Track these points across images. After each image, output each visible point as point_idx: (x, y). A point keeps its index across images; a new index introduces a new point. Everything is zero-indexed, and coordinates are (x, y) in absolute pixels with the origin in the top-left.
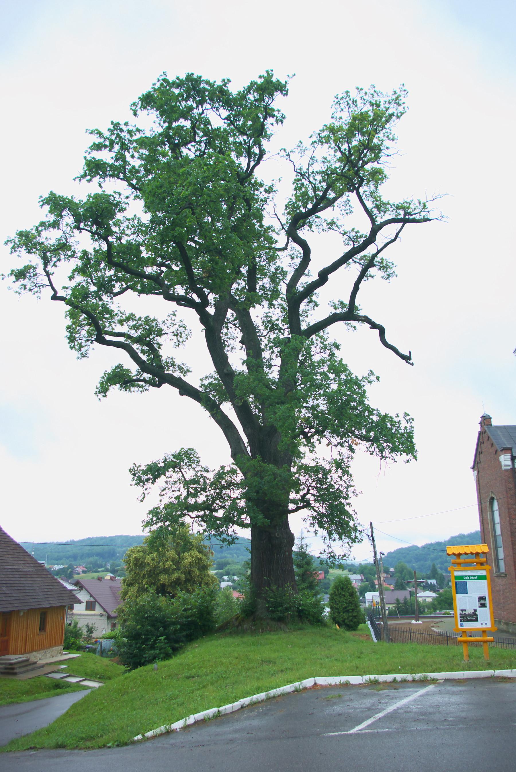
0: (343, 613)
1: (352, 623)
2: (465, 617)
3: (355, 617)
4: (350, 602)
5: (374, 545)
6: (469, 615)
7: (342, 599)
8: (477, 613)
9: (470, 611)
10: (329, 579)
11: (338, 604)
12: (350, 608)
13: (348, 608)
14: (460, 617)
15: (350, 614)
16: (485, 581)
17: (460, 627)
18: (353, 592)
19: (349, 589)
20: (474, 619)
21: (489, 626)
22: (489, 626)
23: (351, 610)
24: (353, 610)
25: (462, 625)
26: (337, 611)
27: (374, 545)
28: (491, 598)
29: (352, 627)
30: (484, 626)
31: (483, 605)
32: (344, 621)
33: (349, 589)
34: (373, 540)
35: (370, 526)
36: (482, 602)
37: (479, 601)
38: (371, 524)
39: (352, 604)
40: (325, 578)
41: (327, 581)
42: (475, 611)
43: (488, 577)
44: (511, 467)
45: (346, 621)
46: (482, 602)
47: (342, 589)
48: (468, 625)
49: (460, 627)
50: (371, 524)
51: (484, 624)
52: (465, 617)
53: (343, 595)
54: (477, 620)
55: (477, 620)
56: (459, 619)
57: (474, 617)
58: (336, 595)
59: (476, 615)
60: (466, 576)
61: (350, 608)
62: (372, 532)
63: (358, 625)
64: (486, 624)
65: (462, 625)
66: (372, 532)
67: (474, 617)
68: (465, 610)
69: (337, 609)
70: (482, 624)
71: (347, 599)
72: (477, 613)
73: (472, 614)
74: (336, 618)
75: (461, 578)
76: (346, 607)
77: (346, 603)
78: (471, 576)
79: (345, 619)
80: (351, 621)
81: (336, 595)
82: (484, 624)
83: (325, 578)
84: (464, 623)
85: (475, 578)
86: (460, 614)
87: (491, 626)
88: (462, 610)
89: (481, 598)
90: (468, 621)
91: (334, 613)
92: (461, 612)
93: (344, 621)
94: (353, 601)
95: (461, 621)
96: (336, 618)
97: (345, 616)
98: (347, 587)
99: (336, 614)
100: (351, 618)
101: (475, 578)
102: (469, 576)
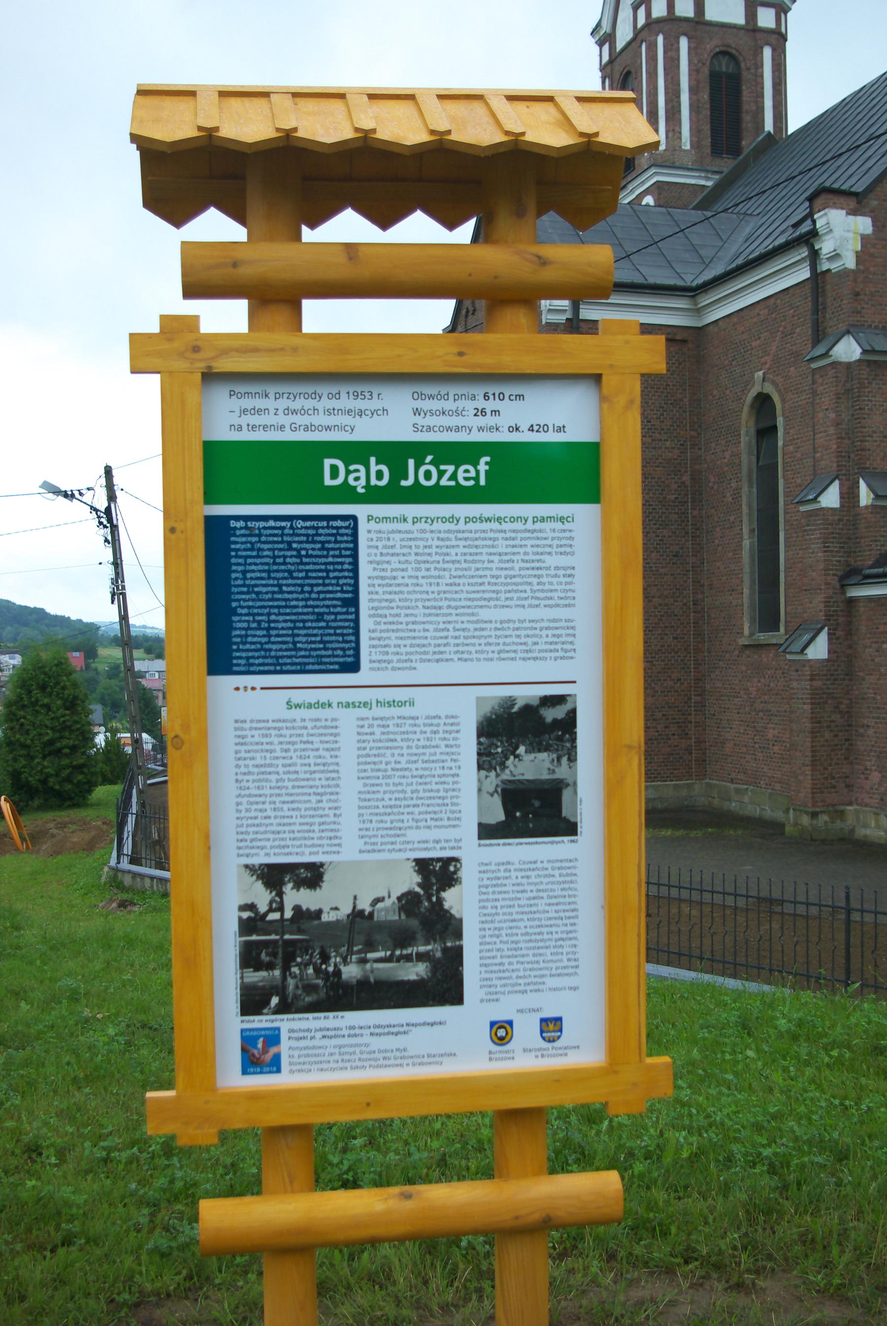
0: (44, 757)
1: (68, 787)
2: (305, 959)
3: (79, 768)
4: (65, 727)
5: (114, 542)
6: (360, 927)
7: (41, 717)
8: (450, 898)
9: (366, 875)
10: (96, 669)
11: (27, 732)
12: (65, 742)
13: (58, 745)
14: (249, 958)
15: (65, 762)
16: (583, 517)
17: (232, 1077)
18: (75, 698)
19: (64, 688)
20: (416, 971)
21: (584, 1049)
22: (584, 1049)
23: (67, 751)
24: (74, 748)
25: (258, 1056)
26: (24, 752)
27: (114, 542)
28: (634, 728)
29: (71, 799)
30: (526, 1057)
31: (533, 811)
32: (44, 782)
33: (64, 688)
34: (114, 528)
35: (103, 481)
36: (530, 765)
37: (486, 760)
38: (108, 471)
39: (72, 732)
40: (88, 667)
41: (91, 674)
42: (439, 873)
43: (623, 472)
44: (569, 315)
45: (52, 781)
46: (530, 765)
47: (43, 688)
48: (338, 1059)
49: (232, 1077)
50: (108, 471)
51: (527, 1031)
52: (305, 959)
53: (43, 706)
54: (444, 987)
55: (444, 987)
56: (227, 978)
57: (412, 951)
58: (24, 707)
59: (447, 927)
60: (355, 452)
61: (65, 742)
62: (112, 497)
63: (90, 791)
64: (551, 1027)
65: (258, 1056)
66: (112, 497)
67: (412, 951)
68: (311, 875)
69: (24, 746)
70: (501, 1032)
71: (57, 718)
72: (450, 898)
73: (388, 911)
74: (20, 773)
75: (294, 466)
76: (51, 742)
77: (52, 729)
78: (418, 450)
79: (49, 775)
80: (68, 779)
81: (24, 707)
82: (527, 1031)
83: (88, 667)
84: (286, 1024)
85: (465, 475)
86: (252, 923)
87: (613, 1047)
88: (273, 876)
89: (524, 728)
90: (341, 997)
91: (15, 760)
92: (262, 897)
93: (44, 782)
94: (76, 722)
95: (252, 1002)
96: (20, 773)
97: (49, 765)
98: (57, 683)
99: (23, 762)
100: (67, 771)
101: (465, 475)
102: (395, 454)
